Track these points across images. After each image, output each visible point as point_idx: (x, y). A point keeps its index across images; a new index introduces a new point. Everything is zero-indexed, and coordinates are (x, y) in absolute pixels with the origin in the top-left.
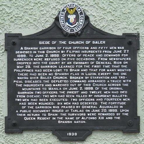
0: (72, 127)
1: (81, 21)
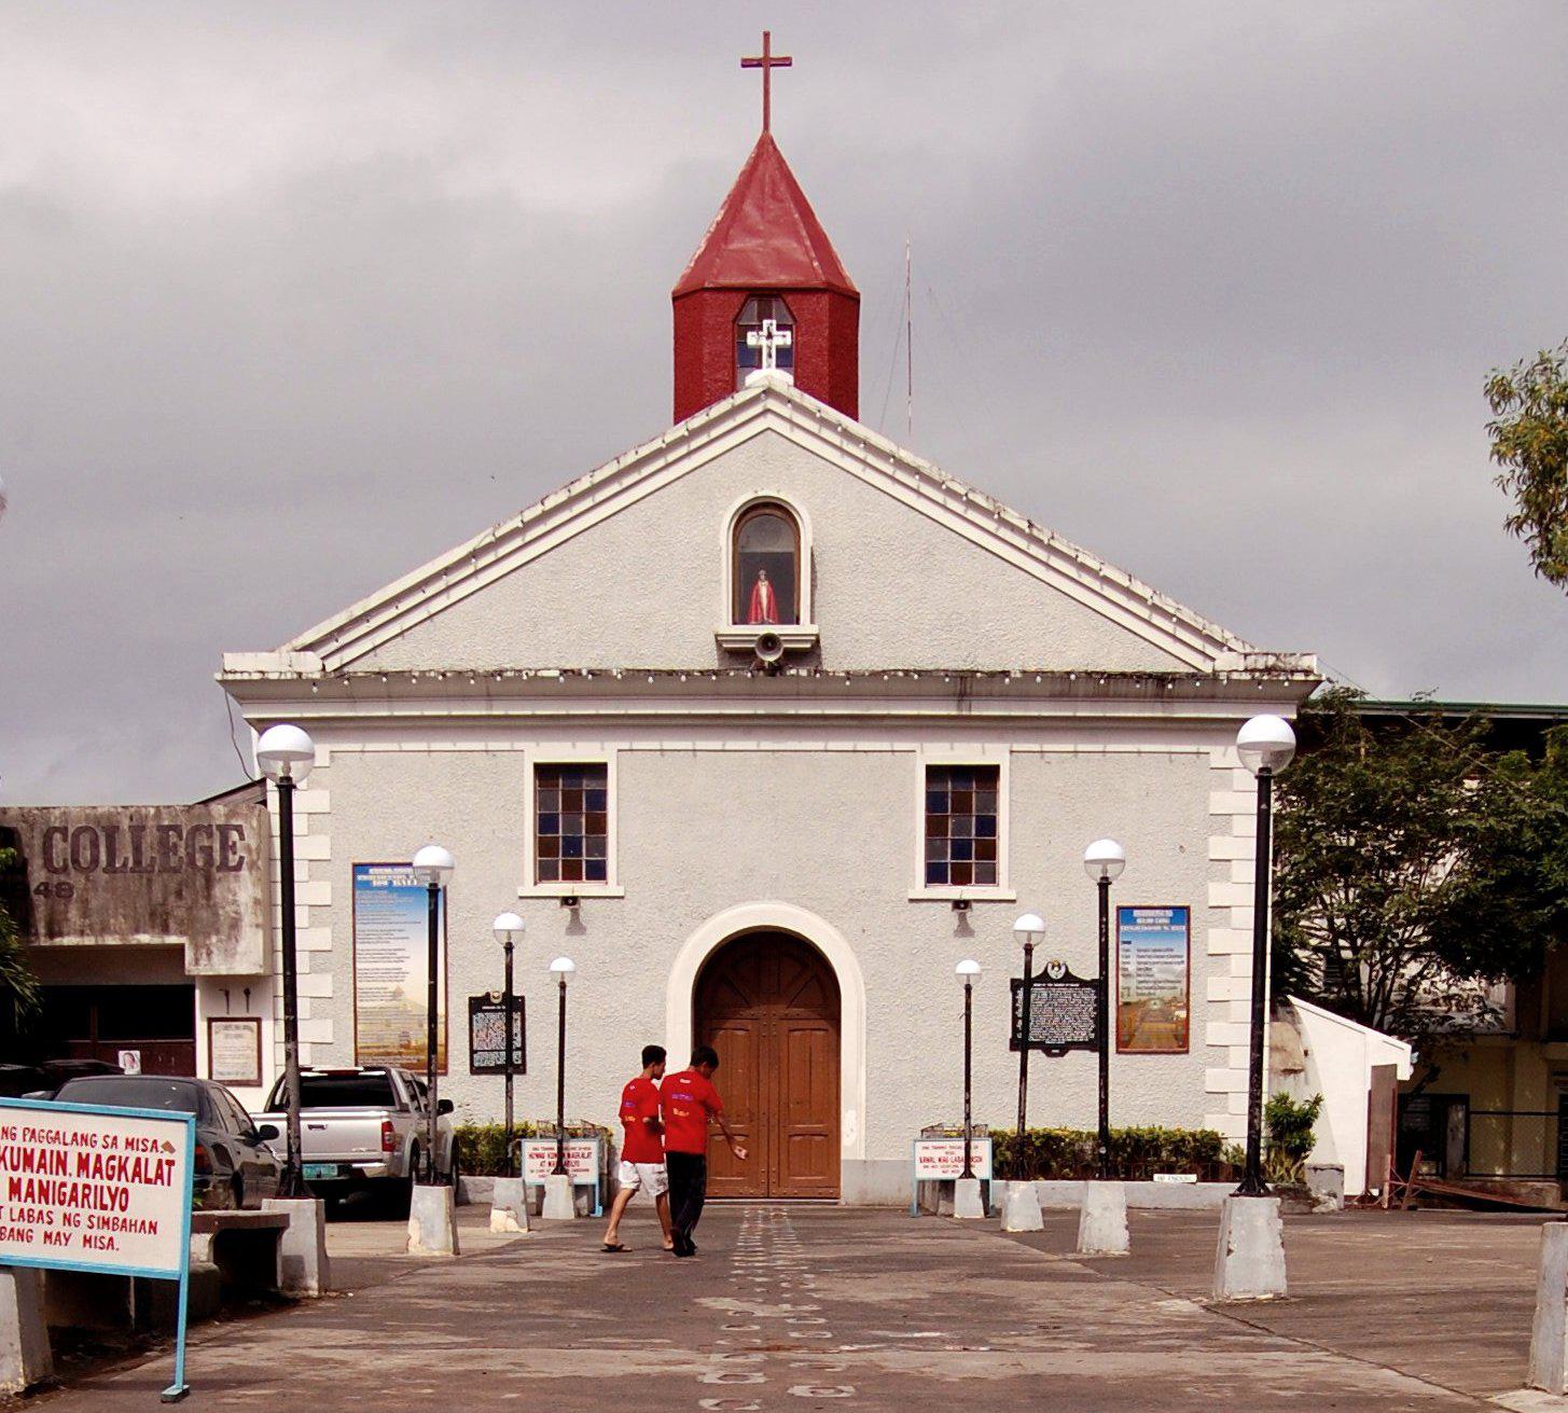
0: (1055, 1046)
1: (1063, 970)
